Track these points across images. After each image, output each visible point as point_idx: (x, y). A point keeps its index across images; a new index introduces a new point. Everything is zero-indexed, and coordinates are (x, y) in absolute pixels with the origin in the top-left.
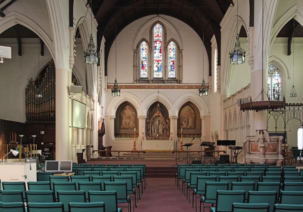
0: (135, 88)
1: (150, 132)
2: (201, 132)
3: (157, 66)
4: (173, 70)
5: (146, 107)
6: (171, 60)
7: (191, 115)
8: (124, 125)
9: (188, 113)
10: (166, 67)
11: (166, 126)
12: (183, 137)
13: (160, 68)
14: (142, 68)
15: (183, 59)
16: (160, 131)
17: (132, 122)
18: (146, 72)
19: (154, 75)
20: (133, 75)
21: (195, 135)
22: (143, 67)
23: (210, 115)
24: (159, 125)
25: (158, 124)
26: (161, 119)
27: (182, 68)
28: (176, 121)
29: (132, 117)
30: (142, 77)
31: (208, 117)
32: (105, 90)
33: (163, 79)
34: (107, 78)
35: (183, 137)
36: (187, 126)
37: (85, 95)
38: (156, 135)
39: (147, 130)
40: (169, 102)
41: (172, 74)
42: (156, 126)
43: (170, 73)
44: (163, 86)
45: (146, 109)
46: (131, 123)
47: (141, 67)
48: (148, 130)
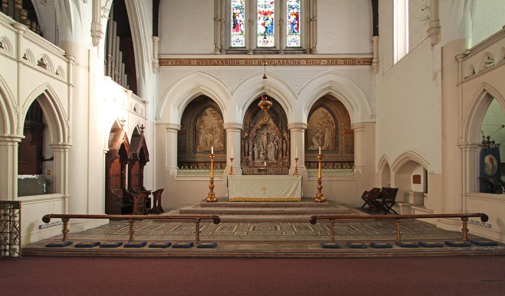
0: (217, 65)
1: (250, 158)
2: (353, 157)
3: (263, 24)
4: (296, 31)
5: (242, 106)
6: (292, 11)
7: (328, 125)
8: (202, 146)
9: (323, 122)
10: (281, 22)
11: (282, 146)
12: (322, 168)
13: (270, 28)
14: (233, 28)
15: (318, 4)
16: (271, 155)
17: (217, 139)
18: (242, 36)
19: (258, 41)
20: (213, 39)
21: (336, 164)
22: (236, 26)
23: (373, 120)
24: (268, 144)
27: (315, 23)
28: (304, 133)
29: (218, 130)
30: (234, 46)
31: (368, 127)
32: (153, 67)
33: (276, 48)
34: (159, 42)
35: (322, 168)
37: (12, 25)
38: (263, 163)
39: (245, 153)
40: (290, 95)
41: (293, 40)
42: (261, 146)
43: (289, 38)
44: (276, 59)
45: (241, 110)
46: (216, 141)
47: (232, 26)
48: (246, 154)
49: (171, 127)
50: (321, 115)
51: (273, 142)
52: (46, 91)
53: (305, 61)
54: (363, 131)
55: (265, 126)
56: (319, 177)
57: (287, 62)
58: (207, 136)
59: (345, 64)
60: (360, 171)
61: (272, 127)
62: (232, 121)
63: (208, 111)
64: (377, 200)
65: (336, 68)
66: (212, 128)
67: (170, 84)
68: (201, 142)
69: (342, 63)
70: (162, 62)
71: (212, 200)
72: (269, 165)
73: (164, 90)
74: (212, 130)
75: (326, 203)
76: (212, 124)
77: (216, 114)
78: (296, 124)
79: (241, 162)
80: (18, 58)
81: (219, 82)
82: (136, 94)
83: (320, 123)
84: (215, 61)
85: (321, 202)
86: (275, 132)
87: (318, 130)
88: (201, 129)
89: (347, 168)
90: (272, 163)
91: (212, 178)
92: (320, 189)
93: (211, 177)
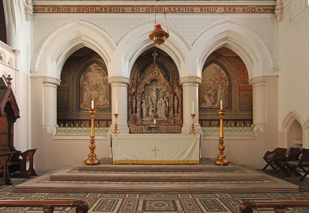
1: (138, 115)
2: (252, 115)
5: (129, 58)
7: (221, 81)
11: (174, 102)
16: (161, 112)
17: (102, 96)
23: (276, 74)
24: (157, 100)
25: (156, 99)
26: (162, 84)
28: (198, 88)
29: (104, 87)
32: (26, 13)
36: (214, 104)
38: (152, 121)
39: (132, 110)
42: (150, 103)
45: (127, 62)
46: (101, 98)
48: (134, 110)
49: (48, 80)
50: (214, 72)
51: (163, 99)
52: (3, 76)
53: (199, 9)
54: (265, 86)
55: (153, 81)
56: (221, 136)
57: (179, 10)
58: (91, 93)
59: (244, 12)
60: (262, 129)
61: (162, 82)
62: (117, 75)
63: (92, 67)
64: (288, 162)
65: (233, 17)
66: (97, 84)
67: (46, 34)
68: (85, 99)
69: (241, 11)
70: (37, 9)
71: (92, 163)
72: (159, 123)
73: (40, 40)
74: (97, 87)
75: (230, 166)
76: (97, 80)
77: (100, 70)
78: (189, 77)
79: (128, 120)
80: (16, 68)
81: (102, 31)
82: (6, 43)
83: (213, 80)
84: (97, 8)
85: (224, 165)
86: (165, 88)
87: (210, 88)
88: (85, 85)
89: (240, 126)
90: (162, 121)
91: (93, 137)
92: (222, 150)
93: (92, 136)
